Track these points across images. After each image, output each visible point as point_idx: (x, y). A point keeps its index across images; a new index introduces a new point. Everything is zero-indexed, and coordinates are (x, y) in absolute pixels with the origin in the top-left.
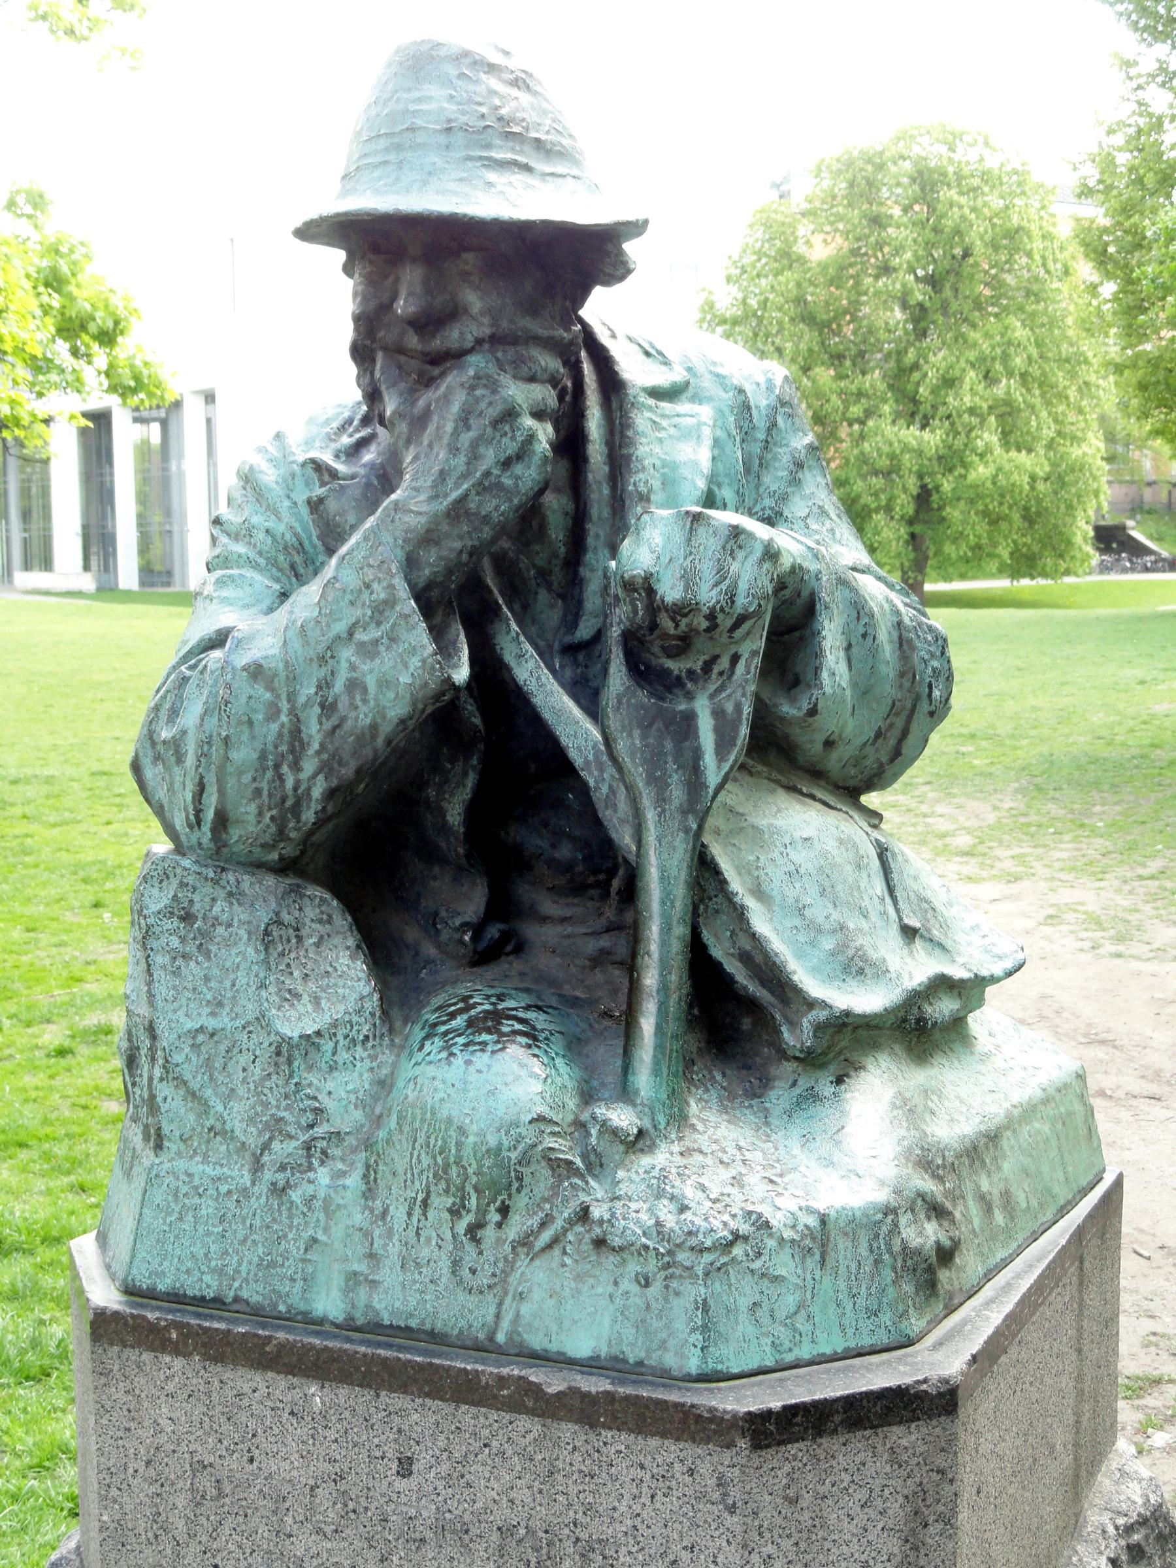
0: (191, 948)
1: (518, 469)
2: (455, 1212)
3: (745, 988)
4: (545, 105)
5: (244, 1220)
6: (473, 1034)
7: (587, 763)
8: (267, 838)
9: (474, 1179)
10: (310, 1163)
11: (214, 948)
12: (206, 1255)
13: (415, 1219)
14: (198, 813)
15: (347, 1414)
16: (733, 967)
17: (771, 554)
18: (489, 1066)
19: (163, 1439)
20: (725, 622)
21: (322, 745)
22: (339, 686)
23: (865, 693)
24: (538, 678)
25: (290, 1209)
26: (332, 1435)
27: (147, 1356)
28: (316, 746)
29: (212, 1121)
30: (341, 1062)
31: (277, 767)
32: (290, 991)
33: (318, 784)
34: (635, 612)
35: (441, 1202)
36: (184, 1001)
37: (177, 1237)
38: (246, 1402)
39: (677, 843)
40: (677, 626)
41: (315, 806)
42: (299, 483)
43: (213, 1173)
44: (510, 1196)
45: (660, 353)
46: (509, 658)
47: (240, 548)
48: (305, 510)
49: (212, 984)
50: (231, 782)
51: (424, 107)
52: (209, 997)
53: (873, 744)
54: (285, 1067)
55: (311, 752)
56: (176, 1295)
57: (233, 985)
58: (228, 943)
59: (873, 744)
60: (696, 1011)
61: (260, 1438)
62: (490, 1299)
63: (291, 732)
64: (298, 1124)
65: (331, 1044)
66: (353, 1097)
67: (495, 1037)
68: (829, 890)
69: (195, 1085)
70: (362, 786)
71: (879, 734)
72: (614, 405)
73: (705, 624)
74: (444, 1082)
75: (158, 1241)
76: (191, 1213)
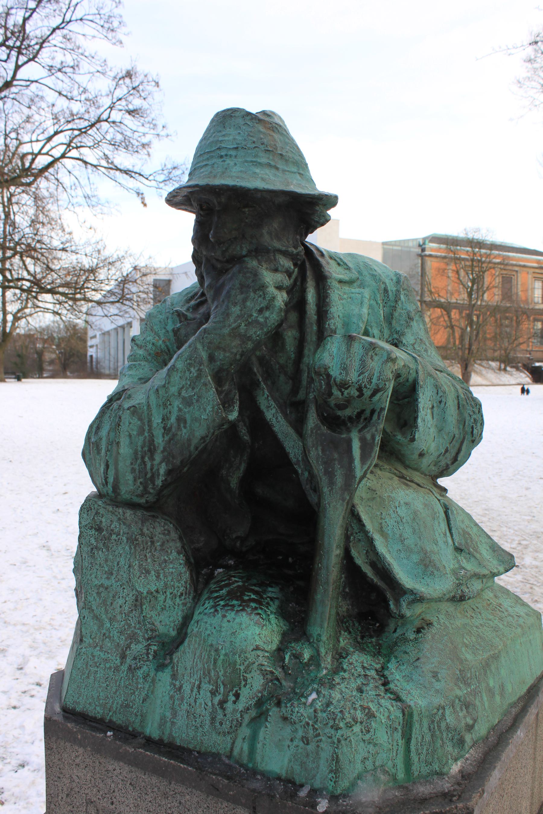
0: (101, 545)
1: (267, 314)
2: (213, 693)
3: (372, 580)
4: (287, 140)
5: (116, 681)
6: (228, 600)
7: (298, 461)
8: (139, 492)
9: (222, 678)
10: (148, 657)
11: (111, 546)
12: (98, 697)
13: (194, 694)
14: (106, 478)
15: (156, 789)
16: (367, 570)
17: (391, 359)
18: (234, 619)
19: (74, 785)
20: (367, 393)
21: (164, 448)
22: (173, 419)
23: (440, 431)
24: (277, 418)
25: (137, 679)
26: (149, 798)
27: (68, 744)
28: (162, 449)
29: (104, 631)
30: (167, 606)
31: (143, 458)
32: (145, 569)
33: (163, 467)
34: (321, 386)
35: (207, 687)
36: (95, 570)
37: (86, 686)
38: (110, 774)
39: (338, 506)
40: (342, 394)
41: (162, 478)
42: (170, 321)
43: (103, 657)
44: (240, 688)
45: (345, 264)
46: (263, 407)
47: (141, 352)
48: (171, 334)
49: (109, 563)
50: (121, 464)
51: (226, 138)
52: (106, 569)
53: (443, 456)
54: (139, 607)
55: (159, 451)
56: (84, 714)
57: (118, 564)
58: (118, 542)
59: (443, 456)
60: (347, 590)
61: (117, 794)
62: (228, 738)
63: (149, 441)
64: (144, 636)
65: (163, 597)
66: (172, 625)
67: (239, 603)
68: (417, 531)
69: (97, 612)
70: (186, 469)
71: (447, 451)
72: (321, 287)
73: (357, 394)
74: (211, 625)
75: (78, 687)
76: (93, 675)
